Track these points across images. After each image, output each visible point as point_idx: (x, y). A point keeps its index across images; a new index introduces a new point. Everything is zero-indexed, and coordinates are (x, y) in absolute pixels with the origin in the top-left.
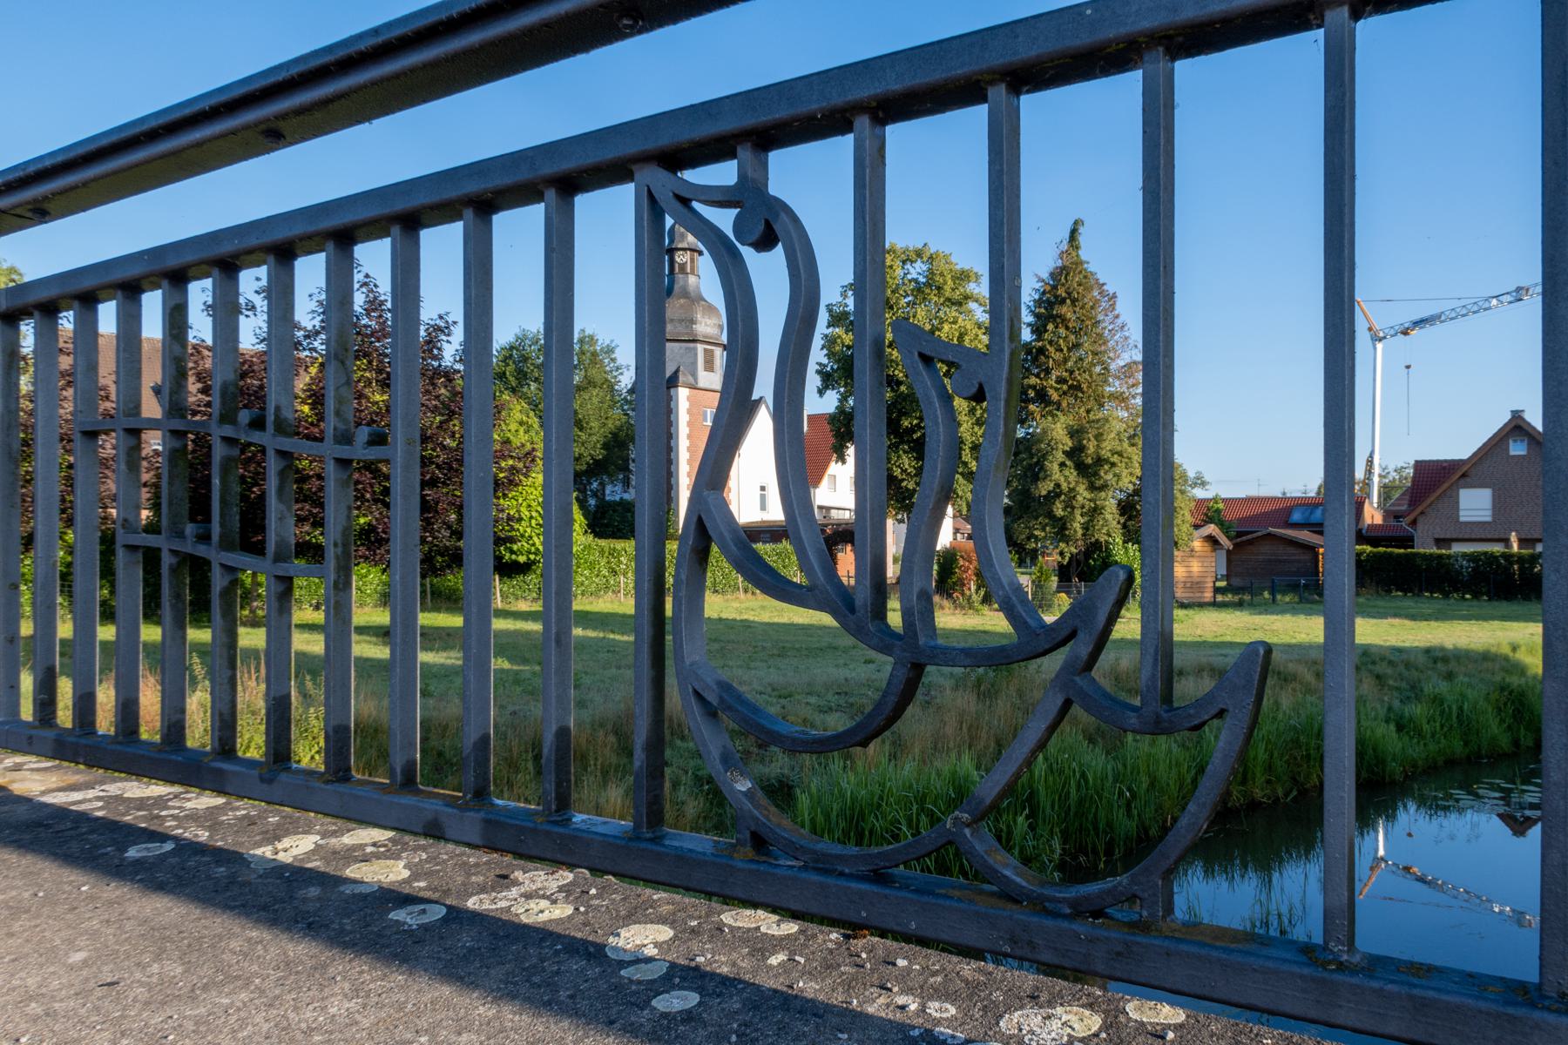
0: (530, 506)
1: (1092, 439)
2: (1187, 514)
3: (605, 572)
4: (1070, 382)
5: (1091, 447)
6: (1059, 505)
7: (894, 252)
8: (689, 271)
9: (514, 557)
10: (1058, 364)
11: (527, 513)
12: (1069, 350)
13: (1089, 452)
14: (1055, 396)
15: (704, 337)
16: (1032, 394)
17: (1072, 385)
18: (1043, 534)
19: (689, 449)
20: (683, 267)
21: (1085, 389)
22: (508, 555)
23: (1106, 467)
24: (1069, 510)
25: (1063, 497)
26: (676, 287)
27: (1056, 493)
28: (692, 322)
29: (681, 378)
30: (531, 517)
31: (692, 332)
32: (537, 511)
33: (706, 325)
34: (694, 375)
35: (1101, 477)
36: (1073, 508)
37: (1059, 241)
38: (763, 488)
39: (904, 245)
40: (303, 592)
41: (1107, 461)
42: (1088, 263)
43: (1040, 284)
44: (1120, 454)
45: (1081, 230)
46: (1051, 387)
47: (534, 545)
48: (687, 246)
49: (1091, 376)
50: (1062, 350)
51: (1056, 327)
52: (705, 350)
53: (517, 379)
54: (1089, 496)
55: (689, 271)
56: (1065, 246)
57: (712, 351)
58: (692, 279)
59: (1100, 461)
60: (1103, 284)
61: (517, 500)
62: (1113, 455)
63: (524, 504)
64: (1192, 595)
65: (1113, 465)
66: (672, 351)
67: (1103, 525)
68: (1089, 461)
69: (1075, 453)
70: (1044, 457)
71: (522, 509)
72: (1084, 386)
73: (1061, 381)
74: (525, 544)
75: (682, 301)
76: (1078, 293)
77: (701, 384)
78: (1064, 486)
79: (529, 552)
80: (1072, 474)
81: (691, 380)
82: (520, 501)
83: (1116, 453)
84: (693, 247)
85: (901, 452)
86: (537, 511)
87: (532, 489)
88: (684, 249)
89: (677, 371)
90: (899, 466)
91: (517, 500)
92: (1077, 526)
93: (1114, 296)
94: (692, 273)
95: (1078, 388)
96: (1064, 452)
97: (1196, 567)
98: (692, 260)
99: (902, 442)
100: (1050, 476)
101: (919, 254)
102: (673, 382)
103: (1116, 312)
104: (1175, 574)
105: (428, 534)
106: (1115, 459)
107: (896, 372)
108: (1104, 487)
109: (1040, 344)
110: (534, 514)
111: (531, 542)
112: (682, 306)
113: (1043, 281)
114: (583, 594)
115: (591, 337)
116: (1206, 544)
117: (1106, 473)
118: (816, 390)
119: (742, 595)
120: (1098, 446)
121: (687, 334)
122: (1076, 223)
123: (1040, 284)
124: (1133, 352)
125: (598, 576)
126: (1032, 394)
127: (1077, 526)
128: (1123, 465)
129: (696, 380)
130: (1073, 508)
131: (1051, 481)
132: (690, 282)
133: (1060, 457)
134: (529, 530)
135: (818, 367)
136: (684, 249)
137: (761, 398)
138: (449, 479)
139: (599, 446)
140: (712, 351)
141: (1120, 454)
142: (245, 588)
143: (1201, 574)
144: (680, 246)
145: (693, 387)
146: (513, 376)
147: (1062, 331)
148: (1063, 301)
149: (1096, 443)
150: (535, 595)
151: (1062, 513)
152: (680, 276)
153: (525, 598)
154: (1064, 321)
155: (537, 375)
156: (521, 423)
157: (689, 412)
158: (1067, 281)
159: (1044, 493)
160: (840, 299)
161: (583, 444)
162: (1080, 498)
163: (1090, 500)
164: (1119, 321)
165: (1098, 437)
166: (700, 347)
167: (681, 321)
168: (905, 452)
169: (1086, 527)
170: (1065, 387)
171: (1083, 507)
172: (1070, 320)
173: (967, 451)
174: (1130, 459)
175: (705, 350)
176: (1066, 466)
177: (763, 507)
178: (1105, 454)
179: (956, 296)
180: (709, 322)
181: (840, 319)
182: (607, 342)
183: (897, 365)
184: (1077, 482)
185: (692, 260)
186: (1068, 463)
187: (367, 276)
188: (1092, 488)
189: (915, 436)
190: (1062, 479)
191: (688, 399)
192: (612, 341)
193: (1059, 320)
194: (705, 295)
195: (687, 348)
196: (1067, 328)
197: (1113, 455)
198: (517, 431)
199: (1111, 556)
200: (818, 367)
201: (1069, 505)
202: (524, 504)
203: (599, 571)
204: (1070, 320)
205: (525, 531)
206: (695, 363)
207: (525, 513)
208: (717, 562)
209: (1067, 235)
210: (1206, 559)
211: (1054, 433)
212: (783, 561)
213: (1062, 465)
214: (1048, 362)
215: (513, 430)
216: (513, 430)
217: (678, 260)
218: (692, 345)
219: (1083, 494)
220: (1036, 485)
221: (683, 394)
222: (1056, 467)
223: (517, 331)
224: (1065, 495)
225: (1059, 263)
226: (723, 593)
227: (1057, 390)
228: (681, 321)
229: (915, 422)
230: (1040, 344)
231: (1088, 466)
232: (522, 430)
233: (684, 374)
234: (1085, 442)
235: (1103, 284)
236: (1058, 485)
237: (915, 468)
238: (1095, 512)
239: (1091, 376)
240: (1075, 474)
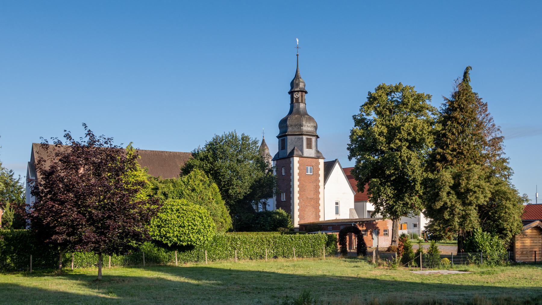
0: (188, 220)
1: (465, 179)
2: (517, 217)
3: (230, 248)
4: (458, 150)
5: (463, 183)
6: (446, 214)
7: (384, 88)
8: (300, 101)
9: (181, 243)
10: (454, 141)
11: (187, 223)
12: (459, 134)
13: (462, 186)
14: (449, 158)
15: (307, 132)
16: (438, 157)
17: (459, 152)
18: (439, 228)
19: (299, 186)
20: (297, 100)
21: (465, 154)
22: (179, 242)
23: (471, 194)
24: (452, 216)
25: (448, 209)
26: (294, 109)
27: (444, 207)
28: (301, 125)
29: (295, 153)
30: (189, 225)
31: (301, 130)
32: (191, 222)
33: (308, 126)
34: (302, 151)
35: (468, 199)
36: (454, 215)
37: (456, 79)
38: (337, 203)
39: (389, 84)
40: (90, 260)
41: (471, 190)
42: (429, 97)
43: (446, 101)
44: (478, 187)
45: (470, 72)
46: (448, 153)
47: (190, 237)
48: (299, 90)
49: (469, 147)
50: (455, 134)
51: (453, 123)
52: (307, 138)
53: (213, 158)
54: (462, 209)
55: (300, 101)
56: (460, 81)
57: (311, 139)
58: (302, 105)
59: (468, 190)
60: (480, 99)
61: (183, 218)
62: (475, 187)
63: (186, 219)
64: (526, 258)
65: (475, 192)
66: (292, 140)
67: (469, 223)
68: (463, 191)
69: (455, 187)
70: (440, 190)
71: (185, 222)
72: (465, 152)
73: (454, 150)
74: (186, 237)
75: (296, 116)
76: (464, 105)
77: (305, 155)
78: (449, 204)
79: (188, 241)
80: (454, 197)
81: (300, 153)
82: (185, 218)
83: (476, 186)
84: (302, 90)
85: (386, 186)
86: (191, 222)
87: (191, 213)
88: (298, 91)
89: (293, 149)
90: (385, 193)
91: (183, 218)
92: (456, 224)
93: (486, 105)
94: (302, 102)
95: (462, 153)
96: (450, 187)
97: (528, 242)
98: (302, 96)
99: (387, 182)
100: (442, 199)
101: (397, 88)
102: (292, 155)
103: (487, 113)
104: (516, 247)
105: (107, 239)
106: (476, 189)
107: (382, 148)
108: (470, 204)
109: (444, 132)
110: (190, 224)
111: (189, 236)
112: (296, 118)
113: (447, 99)
114: (219, 259)
115: (246, 137)
116: (535, 231)
117: (470, 197)
118: (348, 157)
119: (295, 258)
120: (467, 182)
121: (298, 131)
122: (467, 69)
123: (446, 101)
124: (497, 133)
125: (226, 250)
126: (438, 157)
127: (456, 224)
128: (480, 192)
129: (302, 153)
130: (454, 215)
131: (442, 201)
132: (301, 106)
133: (447, 189)
134: (187, 231)
135: (348, 146)
136: (298, 91)
137: (336, 160)
138: (116, 215)
139: (248, 188)
140: (311, 139)
141: (478, 187)
142: (66, 258)
143: (522, 247)
144: (296, 90)
145: (301, 156)
146: (211, 157)
147: (455, 124)
148: (456, 110)
149: (466, 181)
150: (196, 259)
151: (448, 218)
152: (296, 104)
153: (191, 261)
154: (456, 119)
155: (221, 156)
156: (201, 181)
157: (299, 168)
158: (459, 99)
159: (438, 207)
160: (360, 113)
161: (241, 187)
162: (457, 210)
163: (462, 210)
164: (489, 117)
165: (468, 179)
166: (305, 138)
167: (296, 125)
168: (388, 186)
169: (461, 224)
170: (455, 153)
171: (459, 214)
172: (459, 119)
173: (418, 185)
174: (483, 189)
175: (307, 138)
176: (451, 193)
177: (337, 212)
178: (471, 187)
179: (417, 107)
180: (309, 125)
181: (359, 122)
182: (254, 139)
183: (382, 144)
184: (456, 202)
185: (302, 96)
186: (452, 192)
187: (89, 131)
188: (464, 204)
189: (392, 179)
190: (448, 200)
191: (299, 162)
192: (256, 138)
193: (453, 119)
194: (308, 113)
195: (298, 138)
196: (458, 123)
197: (475, 187)
198: (199, 184)
199: (474, 238)
200: (348, 146)
201: (452, 213)
202: (186, 219)
203: (227, 248)
204: (459, 119)
205: (186, 232)
206: (302, 145)
207: (186, 224)
208: (285, 243)
209: (463, 75)
210: (536, 239)
211: (444, 177)
212: (318, 242)
213: (448, 193)
214: (447, 141)
215: (197, 184)
216: (197, 184)
217: (295, 96)
218: (301, 137)
219: (459, 207)
220: (435, 204)
221: (296, 160)
222: (445, 194)
223: (214, 136)
224: (450, 208)
225: (457, 90)
226: (288, 257)
227: (451, 154)
228: (296, 125)
229: (392, 171)
230: (444, 132)
231: (462, 193)
232: (201, 185)
233: (297, 150)
234: (461, 181)
235: (480, 99)
236: (446, 203)
237: (393, 194)
238: (465, 217)
239: (469, 147)
240: (455, 197)
